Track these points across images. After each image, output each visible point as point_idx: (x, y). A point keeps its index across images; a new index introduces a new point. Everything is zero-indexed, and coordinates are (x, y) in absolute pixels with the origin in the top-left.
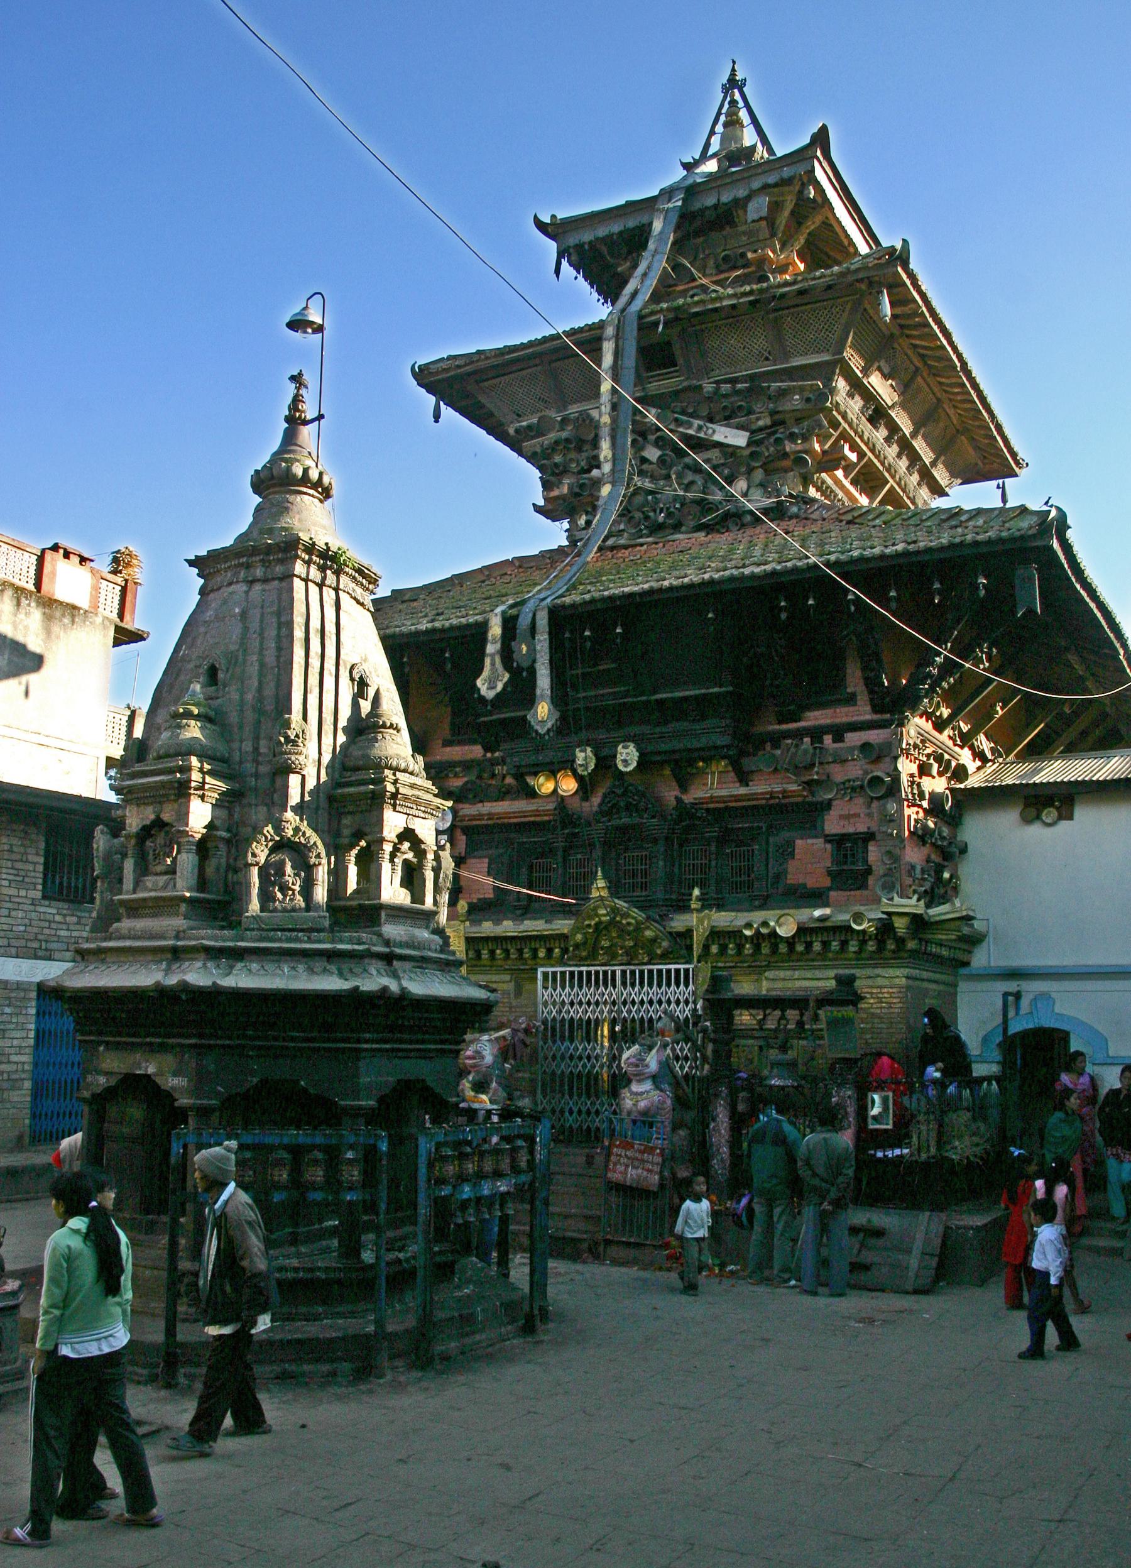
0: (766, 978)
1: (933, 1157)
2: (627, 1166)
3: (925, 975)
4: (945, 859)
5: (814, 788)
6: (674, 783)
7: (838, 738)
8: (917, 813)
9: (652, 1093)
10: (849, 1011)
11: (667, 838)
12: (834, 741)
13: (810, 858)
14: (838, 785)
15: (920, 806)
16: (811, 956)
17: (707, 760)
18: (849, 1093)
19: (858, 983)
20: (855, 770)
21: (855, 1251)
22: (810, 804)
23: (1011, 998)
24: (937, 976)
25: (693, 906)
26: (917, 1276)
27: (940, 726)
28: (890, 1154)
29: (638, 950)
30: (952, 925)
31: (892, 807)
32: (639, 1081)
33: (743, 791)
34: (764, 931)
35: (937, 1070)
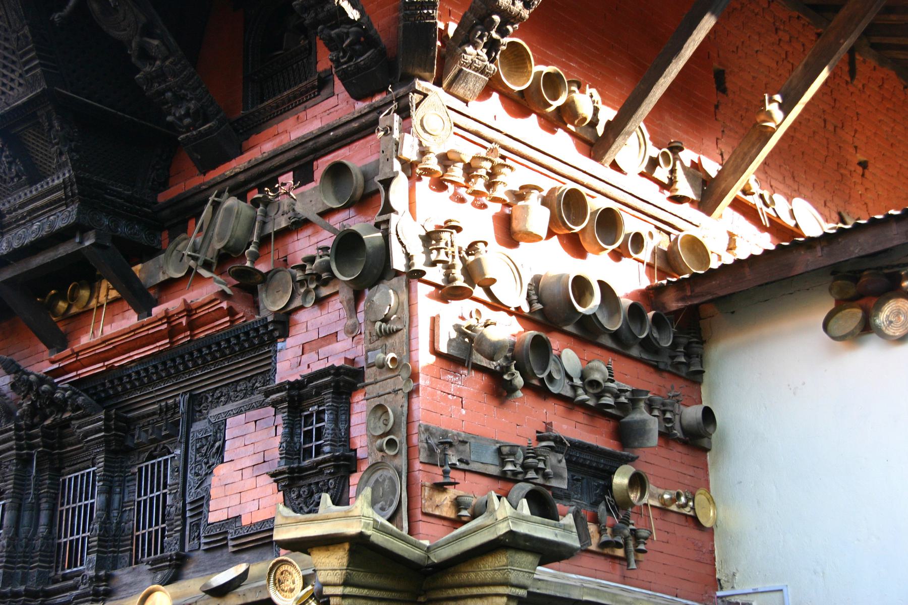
31: (386, 297)
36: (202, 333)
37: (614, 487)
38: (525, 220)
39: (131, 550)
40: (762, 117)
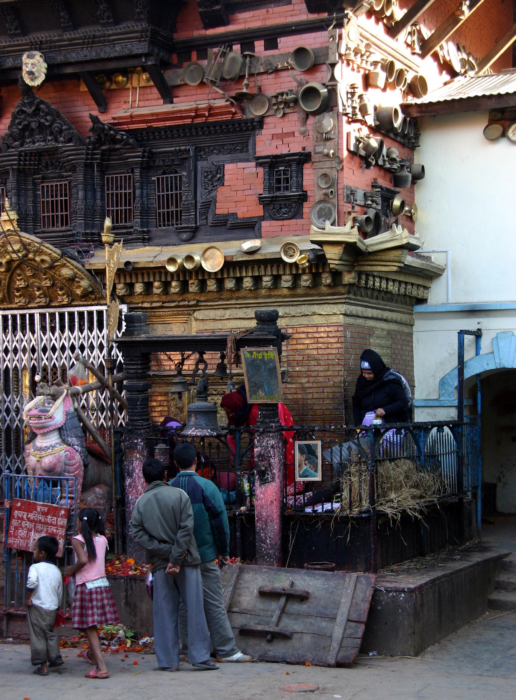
0: (196, 320)
1: (367, 511)
2: (30, 530)
3: (370, 312)
4: (395, 185)
5: (245, 104)
6: (93, 102)
7: (271, 44)
8: (359, 130)
9: (58, 448)
10: (271, 352)
11: (86, 165)
12: (266, 48)
13: (240, 186)
14: (269, 100)
15: (363, 122)
16: (242, 293)
17: (127, 72)
18: (272, 442)
19: (281, 323)
20: (289, 82)
21: (275, 619)
22: (240, 122)
23: (468, 339)
24: (386, 315)
25: (104, 239)
26: (341, 646)
27: (393, 30)
28: (319, 508)
29: (59, 290)
30: (393, 255)
31: (328, 122)
32: (44, 434)
33: (168, 108)
34: (189, 266)
35: (377, 417)
36: (211, 120)
37: (393, 207)
38: (377, 80)
39: (156, 219)
40: (459, 13)
